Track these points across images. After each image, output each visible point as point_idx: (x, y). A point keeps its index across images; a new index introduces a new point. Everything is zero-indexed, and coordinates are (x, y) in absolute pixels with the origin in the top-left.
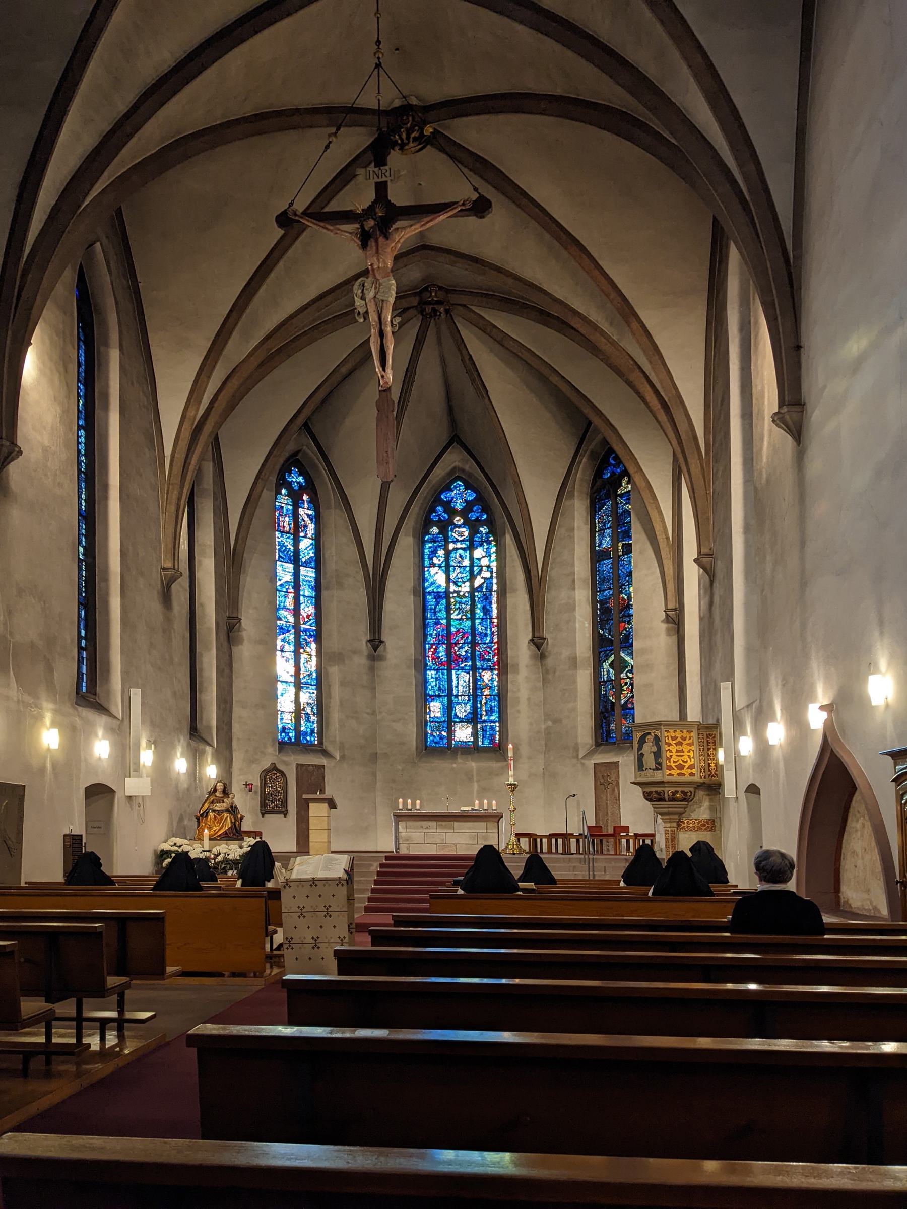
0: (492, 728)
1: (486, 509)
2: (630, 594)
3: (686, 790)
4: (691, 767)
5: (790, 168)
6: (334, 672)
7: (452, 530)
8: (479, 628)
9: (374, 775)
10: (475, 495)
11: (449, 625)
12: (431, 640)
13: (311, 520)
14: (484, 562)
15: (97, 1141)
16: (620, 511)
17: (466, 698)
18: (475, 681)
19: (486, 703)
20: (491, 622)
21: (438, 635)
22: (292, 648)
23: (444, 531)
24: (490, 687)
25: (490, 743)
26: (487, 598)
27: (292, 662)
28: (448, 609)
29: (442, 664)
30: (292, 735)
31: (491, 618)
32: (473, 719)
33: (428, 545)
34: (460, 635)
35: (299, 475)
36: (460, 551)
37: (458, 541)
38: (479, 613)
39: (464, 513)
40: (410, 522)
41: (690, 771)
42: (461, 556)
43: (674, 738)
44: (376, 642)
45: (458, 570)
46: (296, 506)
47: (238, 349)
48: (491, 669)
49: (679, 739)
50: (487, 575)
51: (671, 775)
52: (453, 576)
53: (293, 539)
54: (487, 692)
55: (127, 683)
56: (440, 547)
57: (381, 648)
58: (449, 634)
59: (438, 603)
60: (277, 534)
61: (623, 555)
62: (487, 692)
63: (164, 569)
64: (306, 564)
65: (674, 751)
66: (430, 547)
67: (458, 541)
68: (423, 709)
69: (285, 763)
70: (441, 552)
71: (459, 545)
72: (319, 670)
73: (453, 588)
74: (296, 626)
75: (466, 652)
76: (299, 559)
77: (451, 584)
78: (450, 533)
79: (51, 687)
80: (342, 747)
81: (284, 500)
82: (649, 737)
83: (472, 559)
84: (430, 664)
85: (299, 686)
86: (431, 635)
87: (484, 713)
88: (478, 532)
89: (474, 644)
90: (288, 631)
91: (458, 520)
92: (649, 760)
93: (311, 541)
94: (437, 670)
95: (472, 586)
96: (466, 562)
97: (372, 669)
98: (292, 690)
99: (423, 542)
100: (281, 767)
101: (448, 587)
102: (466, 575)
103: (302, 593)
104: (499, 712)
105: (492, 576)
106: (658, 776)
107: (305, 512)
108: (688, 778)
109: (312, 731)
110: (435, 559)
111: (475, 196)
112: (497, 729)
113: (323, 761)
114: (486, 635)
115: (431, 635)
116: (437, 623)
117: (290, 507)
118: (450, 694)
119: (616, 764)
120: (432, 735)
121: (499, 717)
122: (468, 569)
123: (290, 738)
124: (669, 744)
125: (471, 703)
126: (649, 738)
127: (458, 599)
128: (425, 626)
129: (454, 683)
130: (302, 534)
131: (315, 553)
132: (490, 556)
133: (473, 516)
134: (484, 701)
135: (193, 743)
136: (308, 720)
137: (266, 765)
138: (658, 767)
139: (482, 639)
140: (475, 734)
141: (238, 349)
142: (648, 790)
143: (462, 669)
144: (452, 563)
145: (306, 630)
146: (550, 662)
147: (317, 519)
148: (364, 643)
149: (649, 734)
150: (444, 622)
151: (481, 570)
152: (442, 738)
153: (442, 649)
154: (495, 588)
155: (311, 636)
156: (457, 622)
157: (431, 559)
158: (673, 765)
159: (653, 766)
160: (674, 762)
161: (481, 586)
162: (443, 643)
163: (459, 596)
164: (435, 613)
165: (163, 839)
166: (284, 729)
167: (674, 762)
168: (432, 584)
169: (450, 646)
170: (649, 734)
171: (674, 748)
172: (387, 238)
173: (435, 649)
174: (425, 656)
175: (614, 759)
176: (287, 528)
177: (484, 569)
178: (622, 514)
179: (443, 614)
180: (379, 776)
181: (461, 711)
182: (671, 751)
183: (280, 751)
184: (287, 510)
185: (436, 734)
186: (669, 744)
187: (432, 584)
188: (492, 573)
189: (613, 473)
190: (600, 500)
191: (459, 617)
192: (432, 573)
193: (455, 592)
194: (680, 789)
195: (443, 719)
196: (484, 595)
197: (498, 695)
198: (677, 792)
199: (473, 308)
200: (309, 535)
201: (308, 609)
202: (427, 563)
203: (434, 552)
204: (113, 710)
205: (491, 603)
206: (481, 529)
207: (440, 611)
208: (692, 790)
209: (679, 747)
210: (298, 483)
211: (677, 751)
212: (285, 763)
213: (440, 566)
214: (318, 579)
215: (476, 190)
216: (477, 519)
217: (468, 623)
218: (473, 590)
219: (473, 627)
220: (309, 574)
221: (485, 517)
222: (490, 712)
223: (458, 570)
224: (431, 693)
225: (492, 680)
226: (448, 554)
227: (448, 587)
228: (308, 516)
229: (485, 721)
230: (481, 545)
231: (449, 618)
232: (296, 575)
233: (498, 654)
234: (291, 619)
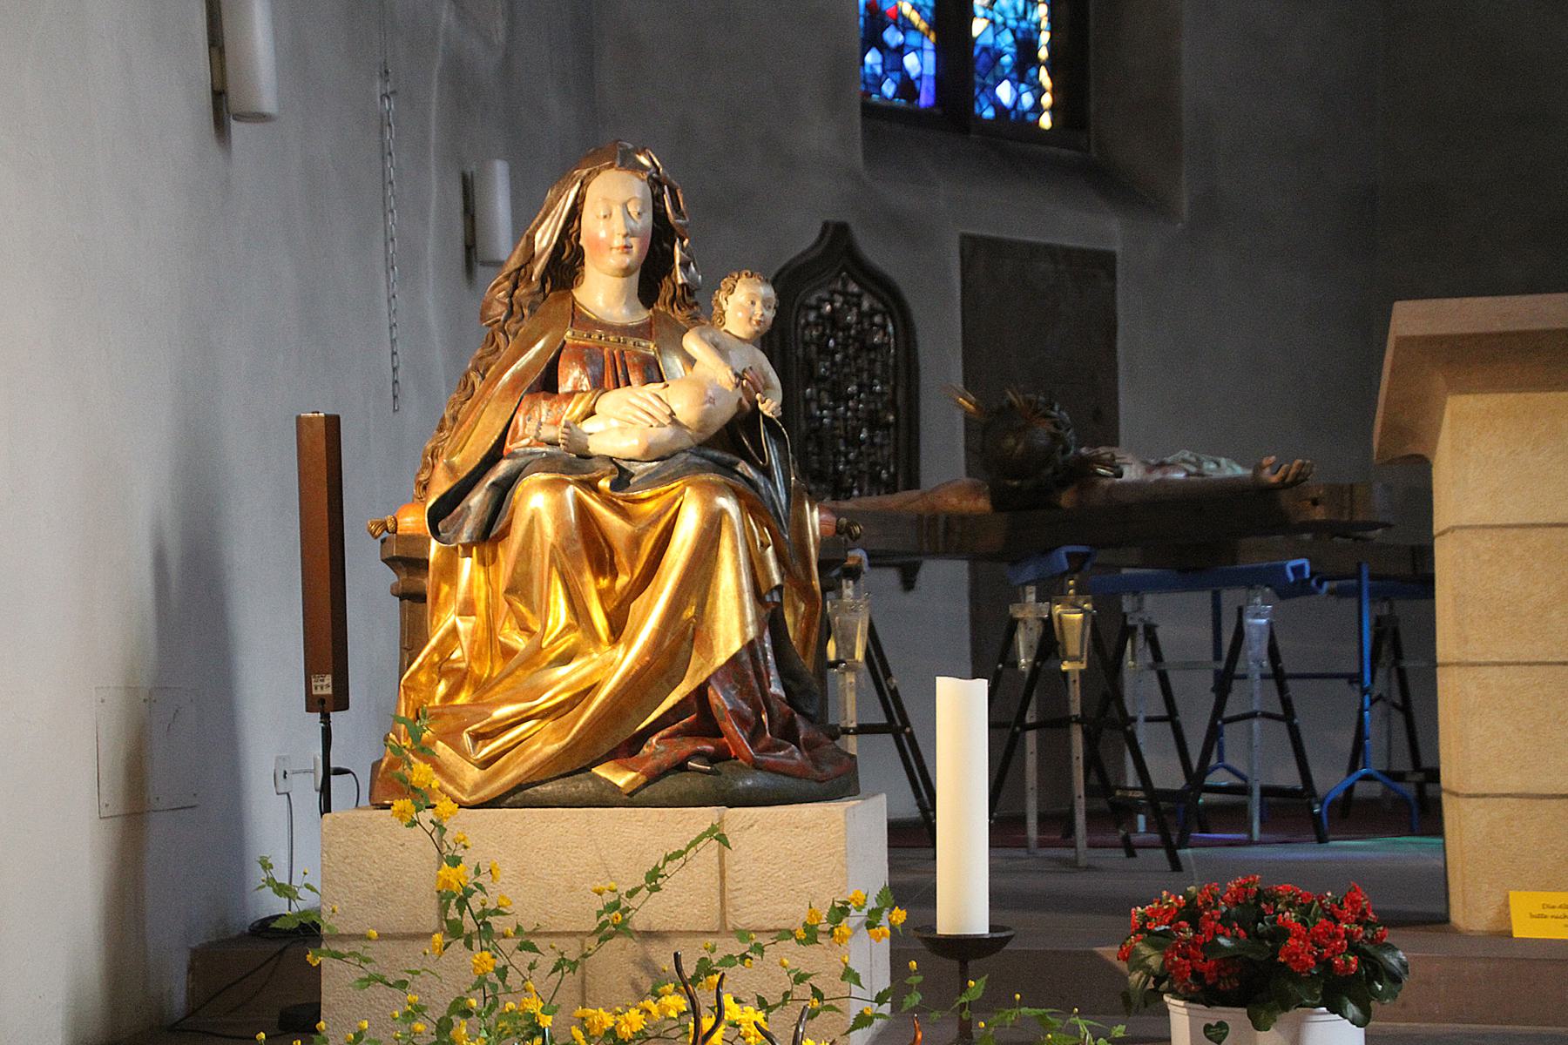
109: (1026, 46)
123: (908, 87)
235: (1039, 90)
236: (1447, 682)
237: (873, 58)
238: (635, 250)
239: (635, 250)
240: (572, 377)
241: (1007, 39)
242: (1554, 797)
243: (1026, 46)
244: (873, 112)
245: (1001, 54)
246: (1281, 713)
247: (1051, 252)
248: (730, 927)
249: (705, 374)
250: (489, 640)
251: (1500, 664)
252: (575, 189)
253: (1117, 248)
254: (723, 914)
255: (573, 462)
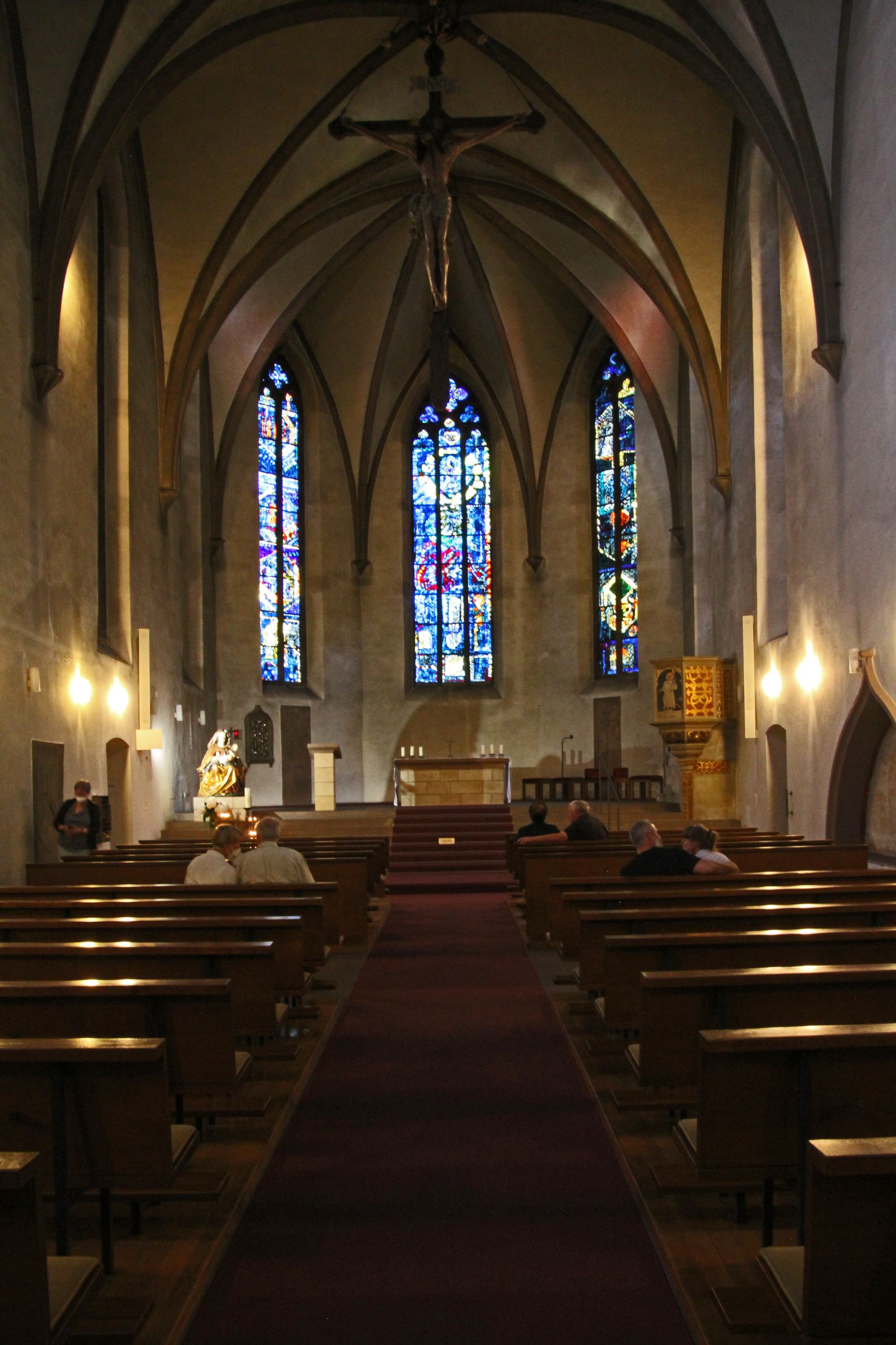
0: (485, 661)
1: (477, 411)
2: (632, 509)
3: (704, 730)
4: (710, 706)
5: (830, 105)
6: (317, 598)
7: (442, 434)
8: (471, 546)
9: (360, 717)
10: (466, 395)
11: (438, 543)
12: (419, 560)
13: (294, 423)
14: (477, 470)
16: (621, 417)
17: (457, 626)
18: (467, 606)
19: (478, 633)
20: (484, 539)
21: (427, 554)
22: (275, 572)
23: (434, 436)
24: (483, 614)
25: (482, 678)
26: (479, 511)
27: (274, 588)
28: (438, 524)
29: (432, 588)
30: (275, 672)
31: (484, 535)
32: (465, 650)
33: (417, 451)
34: (451, 554)
35: (282, 372)
36: (451, 458)
37: (448, 446)
38: (471, 529)
39: (455, 415)
40: (398, 426)
41: (708, 710)
42: (451, 464)
43: (694, 675)
44: (362, 563)
45: (448, 479)
46: (279, 408)
47: (244, 243)
48: (483, 593)
49: (699, 676)
50: (478, 484)
51: (691, 715)
52: (443, 486)
53: (276, 446)
54: (479, 619)
55: (137, 624)
56: (429, 452)
57: (367, 569)
58: (439, 555)
59: (427, 518)
60: (261, 441)
61: (625, 465)
62: (479, 619)
63: (162, 490)
64: (289, 474)
65: (694, 689)
66: (419, 454)
67: (448, 446)
69: (270, 705)
70: (430, 459)
71: (449, 451)
72: (302, 598)
73: (443, 500)
74: (279, 547)
75: (458, 574)
76: (282, 469)
77: (442, 496)
78: (440, 437)
79: (78, 630)
80: (327, 684)
81: (266, 402)
82: (668, 674)
83: (463, 467)
85: (281, 616)
86: (420, 554)
87: (476, 644)
88: (471, 437)
89: (465, 565)
90: (270, 552)
91: (449, 423)
92: (670, 699)
93: (294, 448)
94: (427, 595)
95: (463, 498)
96: (458, 471)
97: (357, 594)
98: (275, 621)
99: (412, 448)
100: (266, 710)
101: (438, 500)
102: (457, 486)
103: (284, 508)
104: (493, 643)
105: (484, 488)
106: (677, 716)
107: (288, 414)
108: (706, 717)
109: (295, 668)
110: (423, 466)
111: (529, 111)
112: (490, 662)
113: (309, 703)
114: (478, 554)
115: (420, 554)
116: (426, 540)
117: (273, 410)
118: (440, 623)
119: (617, 700)
120: (420, 669)
121: (492, 649)
122: (459, 478)
123: (272, 677)
124: (689, 682)
125: (462, 632)
126: (670, 676)
127: (448, 513)
128: (413, 544)
129: (444, 610)
130: (284, 440)
131: (299, 462)
132: (483, 463)
133: (465, 418)
134: (476, 630)
135: (186, 686)
136: (291, 656)
137: (251, 707)
138: (679, 706)
139: (474, 559)
140: (467, 668)
141: (244, 243)
142: (667, 731)
143: (453, 593)
144: (442, 472)
145: (288, 551)
146: (548, 585)
147: (301, 423)
148: (349, 565)
149: (670, 671)
150: (434, 539)
151: (473, 480)
152: (431, 673)
153: (432, 570)
154: (488, 500)
155: (292, 558)
156: (448, 539)
157: (419, 466)
158: (693, 704)
159: (673, 704)
160: (694, 701)
161: (473, 499)
162: (433, 564)
163: (450, 510)
164: (424, 529)
166: (266, 665)
167: (694, 701)
168: (421, 495)
169: (440, 567)
170: (670, 671)
171: (694, 686)
172: (442, 151)
173: (424, 571)
174: (412, 578)
175: (614, 694)
176: (269, 434)
177: (477, 478)
178: (623, 421)
179: (432, 530)
180: (366, 717)
181: (453, 641)
182: (690, 689)
183: (264, 691)
184: (270, 413)
185: (425, 668)
186: (689, 682)
187: (421, 495)
188: (484, 482)
189: (613, 375)
190: (599, 404)
191: (450, 533)
192: (421, 484)
193: (446, 505)
194: (698, 730)
195: (432, 651)
196: (476, 508)
197: (491, 622)
198: (695, 733)
199: (482, 197)
200: (292, 441)
201: (290, 527)
202: (415, 471)
203: (423, 459)
204: (123, 654)
205: (483, 517)
206: (473, 433)
207: (430, 526)
208: (709, 730)
209: (700, 685)
210: (281, 381)
211: (697, 689)
212: (270, 705)
213: (430, 475)
214: (301, 492)
215: (530, 105)
216: (470, 422)
217: (460, 540)
218: (465, 502)
219: (465, 546)
220: (291, 485)
221: (477, 419)
222: (482, 642)
223: (448, 479)
224: (420, 621)
225: (484, 606)
226: (438, 460)
227: (438, 500)
228: (291, 418)
229: (477, 653)
230: (473, 450)
231: (439, 535)
232: (279, 487)
233: (491, 576)
234: (273, 538)
236: (464, 803)
237: (266, 672)
240: (218, 754)
243: (295, 668)
244: (265, 683)
246: (467, 499)
247: (298, 707)
249: (231, 755)
250: (209, 781)
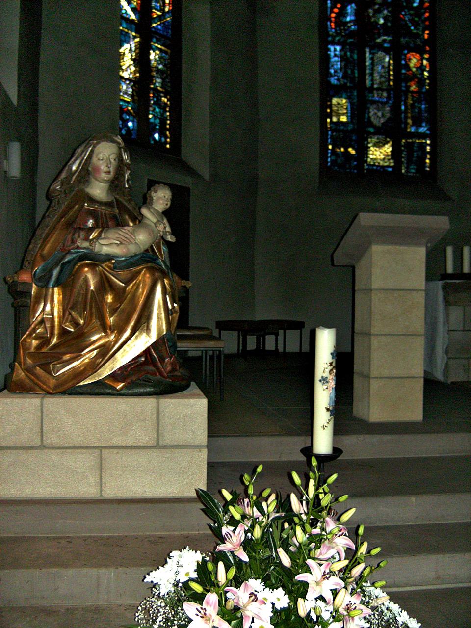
15: (398, 217)
18: (398, 67)
68: (325, 109)
84: (332, 32)
87: (410, 121)
165: (19, 267)
181: (377, 116)
225: (421, 68)
235: (166, 137)
238: (112, 173)
239: (112, 173)
241: (158, 121)
242: (397, 378)
245: (156, 125)
248: (161, 444)
251: (385, 335)
252: (91, 148)
253: (190, 186)
254: (158, 439)
255: (96, 260)
